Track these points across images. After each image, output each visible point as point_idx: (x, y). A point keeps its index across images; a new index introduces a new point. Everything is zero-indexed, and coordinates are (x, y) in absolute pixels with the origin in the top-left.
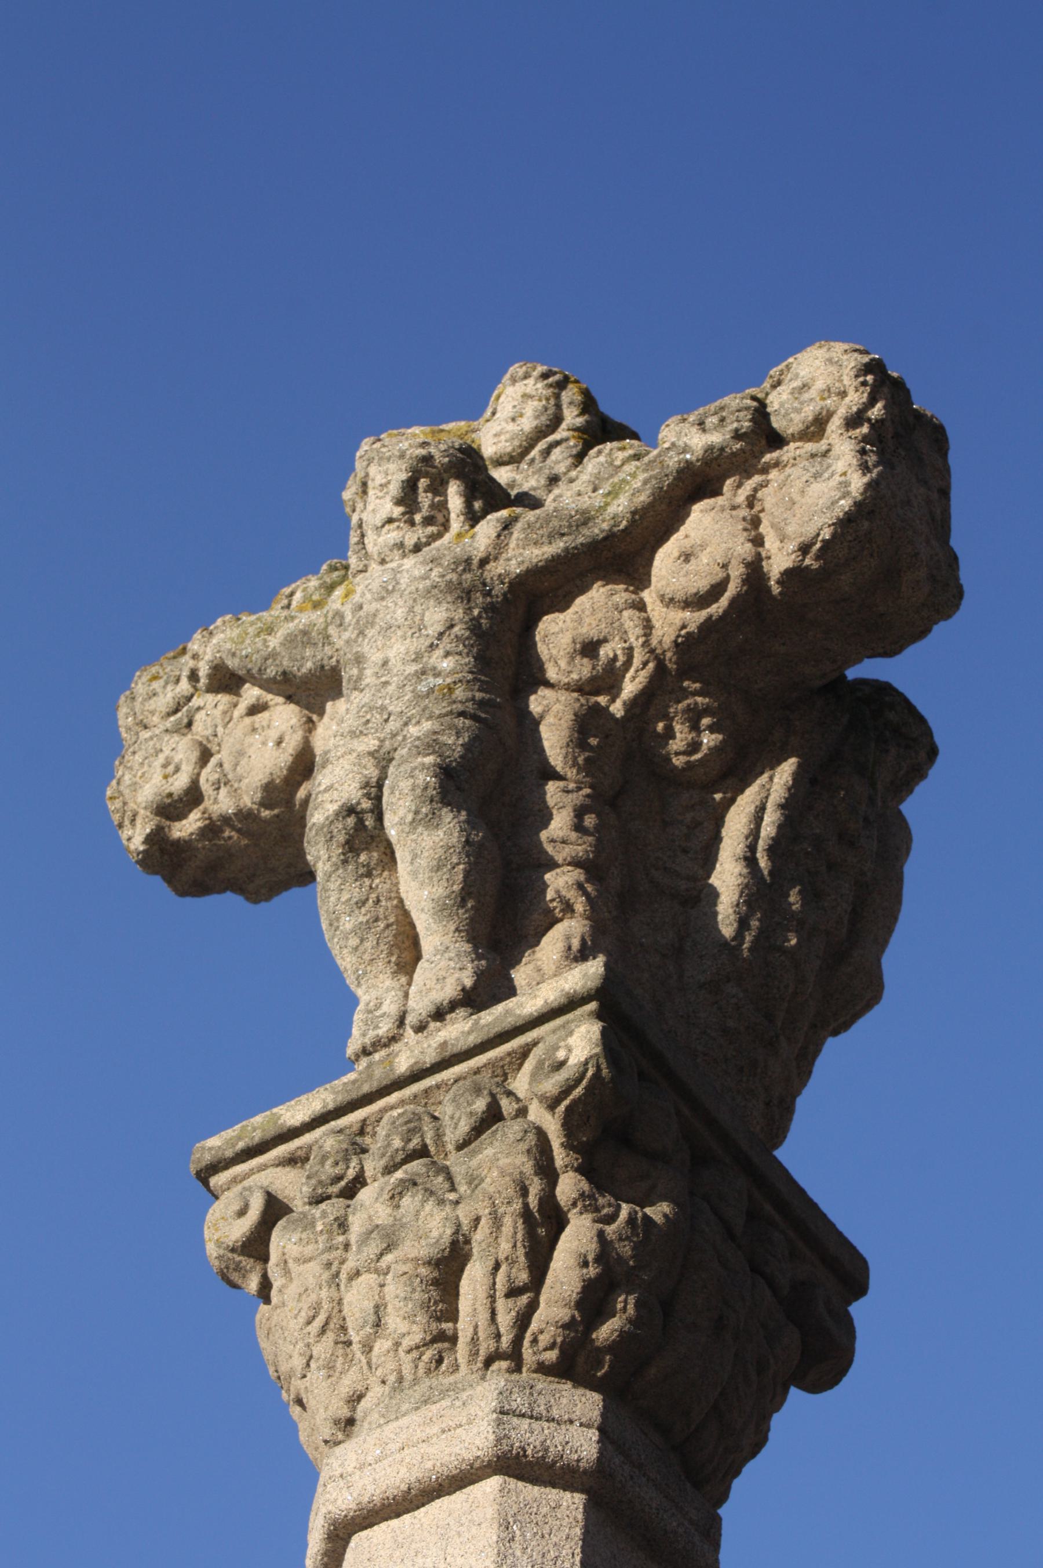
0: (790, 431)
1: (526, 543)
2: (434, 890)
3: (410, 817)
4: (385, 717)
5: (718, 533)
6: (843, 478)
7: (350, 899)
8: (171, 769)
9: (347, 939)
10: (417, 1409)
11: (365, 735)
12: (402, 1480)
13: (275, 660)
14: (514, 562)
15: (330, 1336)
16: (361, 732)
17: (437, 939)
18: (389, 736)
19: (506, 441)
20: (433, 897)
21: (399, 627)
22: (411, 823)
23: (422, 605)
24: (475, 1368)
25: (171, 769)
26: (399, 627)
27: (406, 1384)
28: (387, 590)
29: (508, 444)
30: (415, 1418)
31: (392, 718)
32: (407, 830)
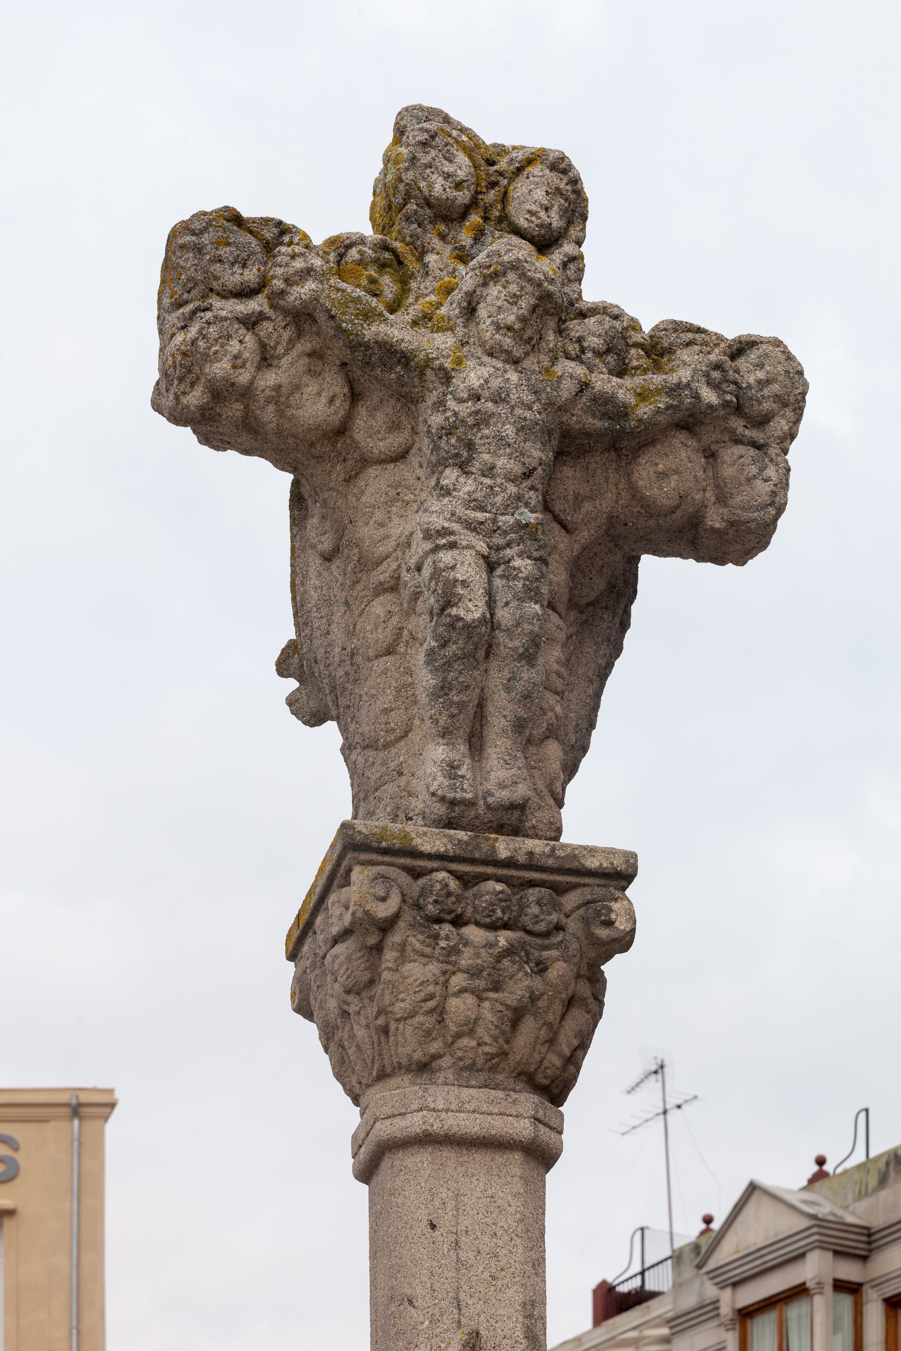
0: (746, 411)
1: (587, 410)
2: (519, 710)
3: (521, 650)
4: (495, 528)
5: (688, 471)
6: (774, 489)
7: (464, 682)
8: (239, 362)
9: (451, 706)
10: (480, 1087)
11: (477, 532)
12: (476, 1134)
13: (366, 350)
14: (575, 418)
15: (435, 1016)
16: (475, 528)
17: (509, 743)
18: (495, 547)
19: (537, 226)
20: (516, 714)
21: (509, 445)
22: (521, 655)
23: (526, 434)
24: (513, 1075)
25: (239, 362)
26: (509, 445)
27: (475, 1068)
28: (501, 397)
29: (537, 229)
30: (482, 1093)
31: (498, 532)
32: (516, 657)
